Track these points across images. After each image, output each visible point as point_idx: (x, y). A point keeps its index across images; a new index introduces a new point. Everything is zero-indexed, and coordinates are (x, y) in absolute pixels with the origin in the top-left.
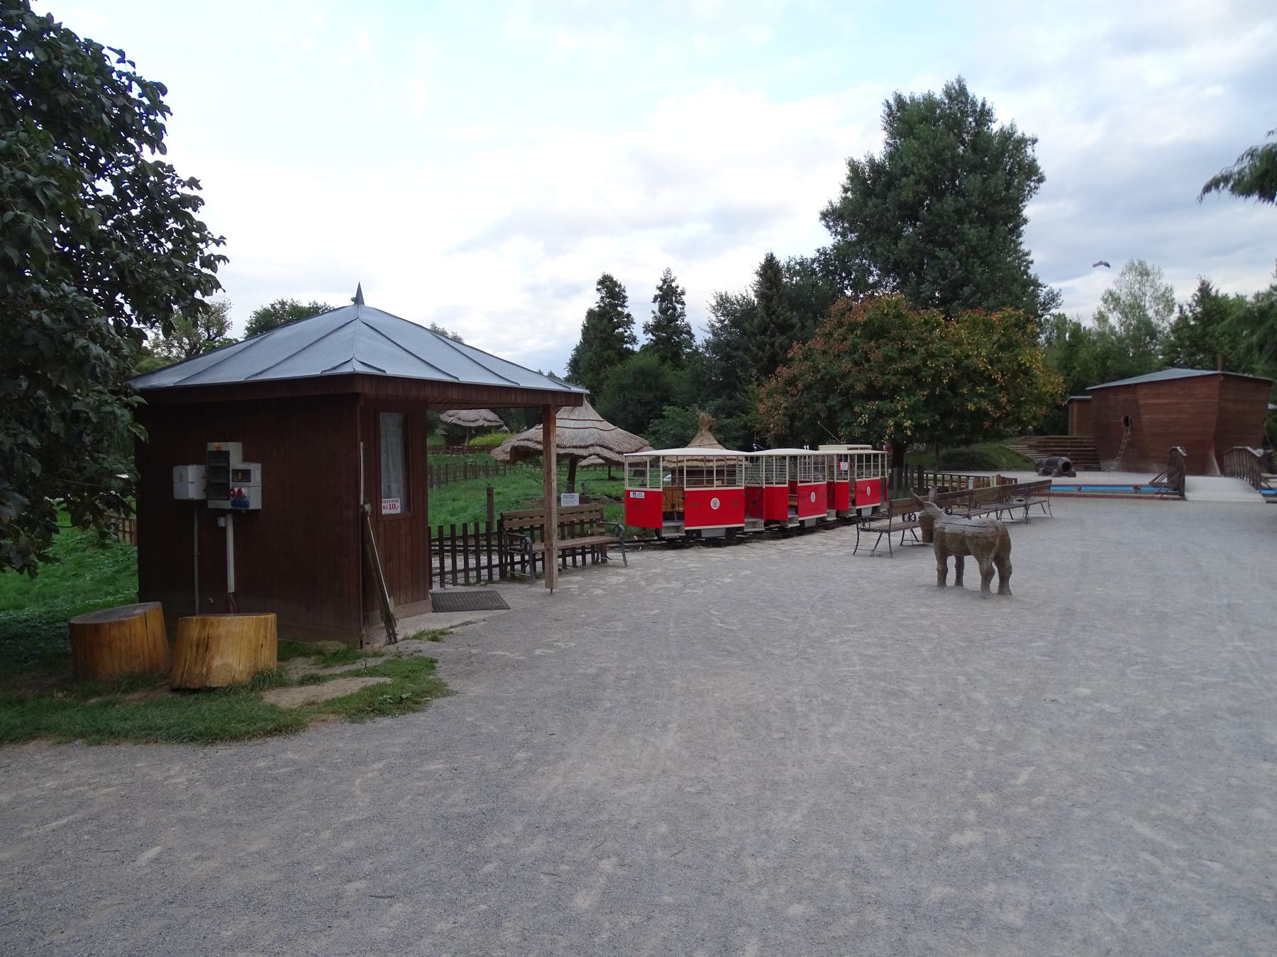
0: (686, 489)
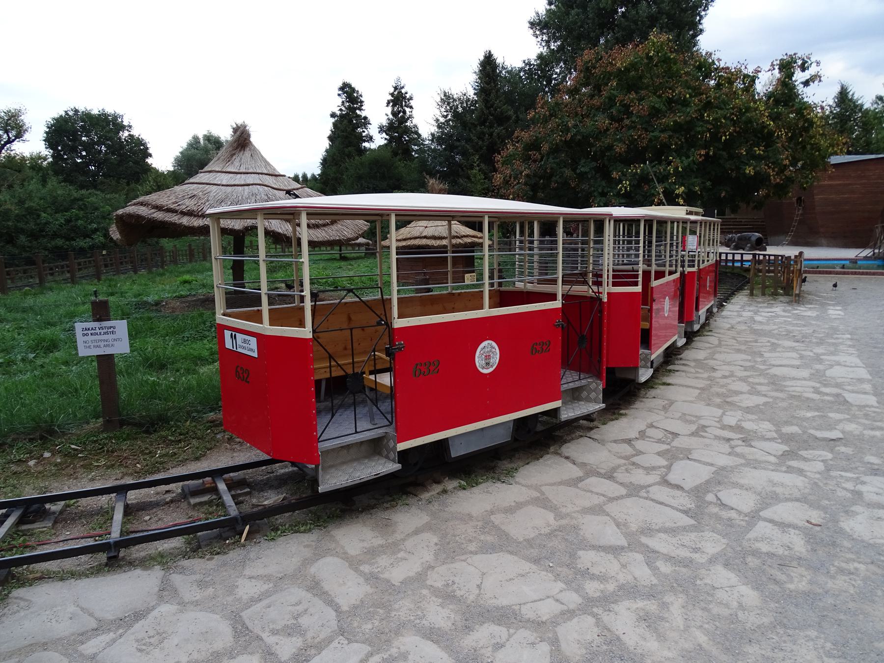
0: (399, 323)
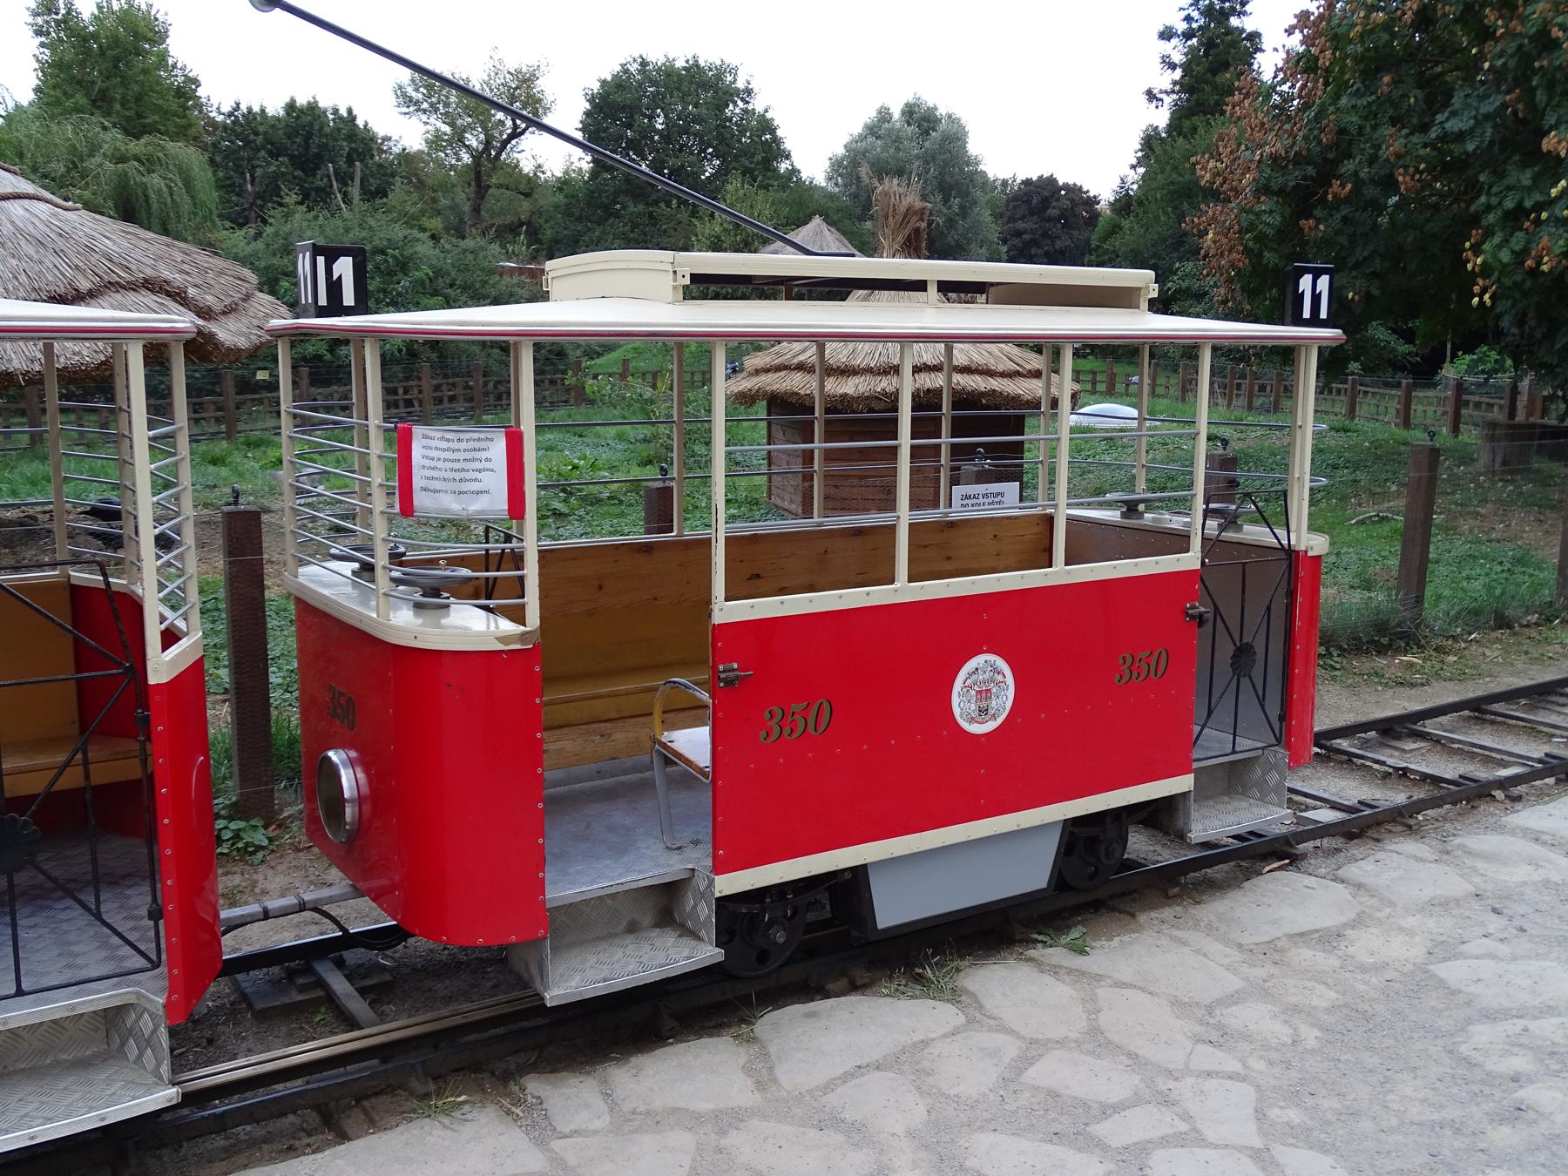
0: (727, 611)
